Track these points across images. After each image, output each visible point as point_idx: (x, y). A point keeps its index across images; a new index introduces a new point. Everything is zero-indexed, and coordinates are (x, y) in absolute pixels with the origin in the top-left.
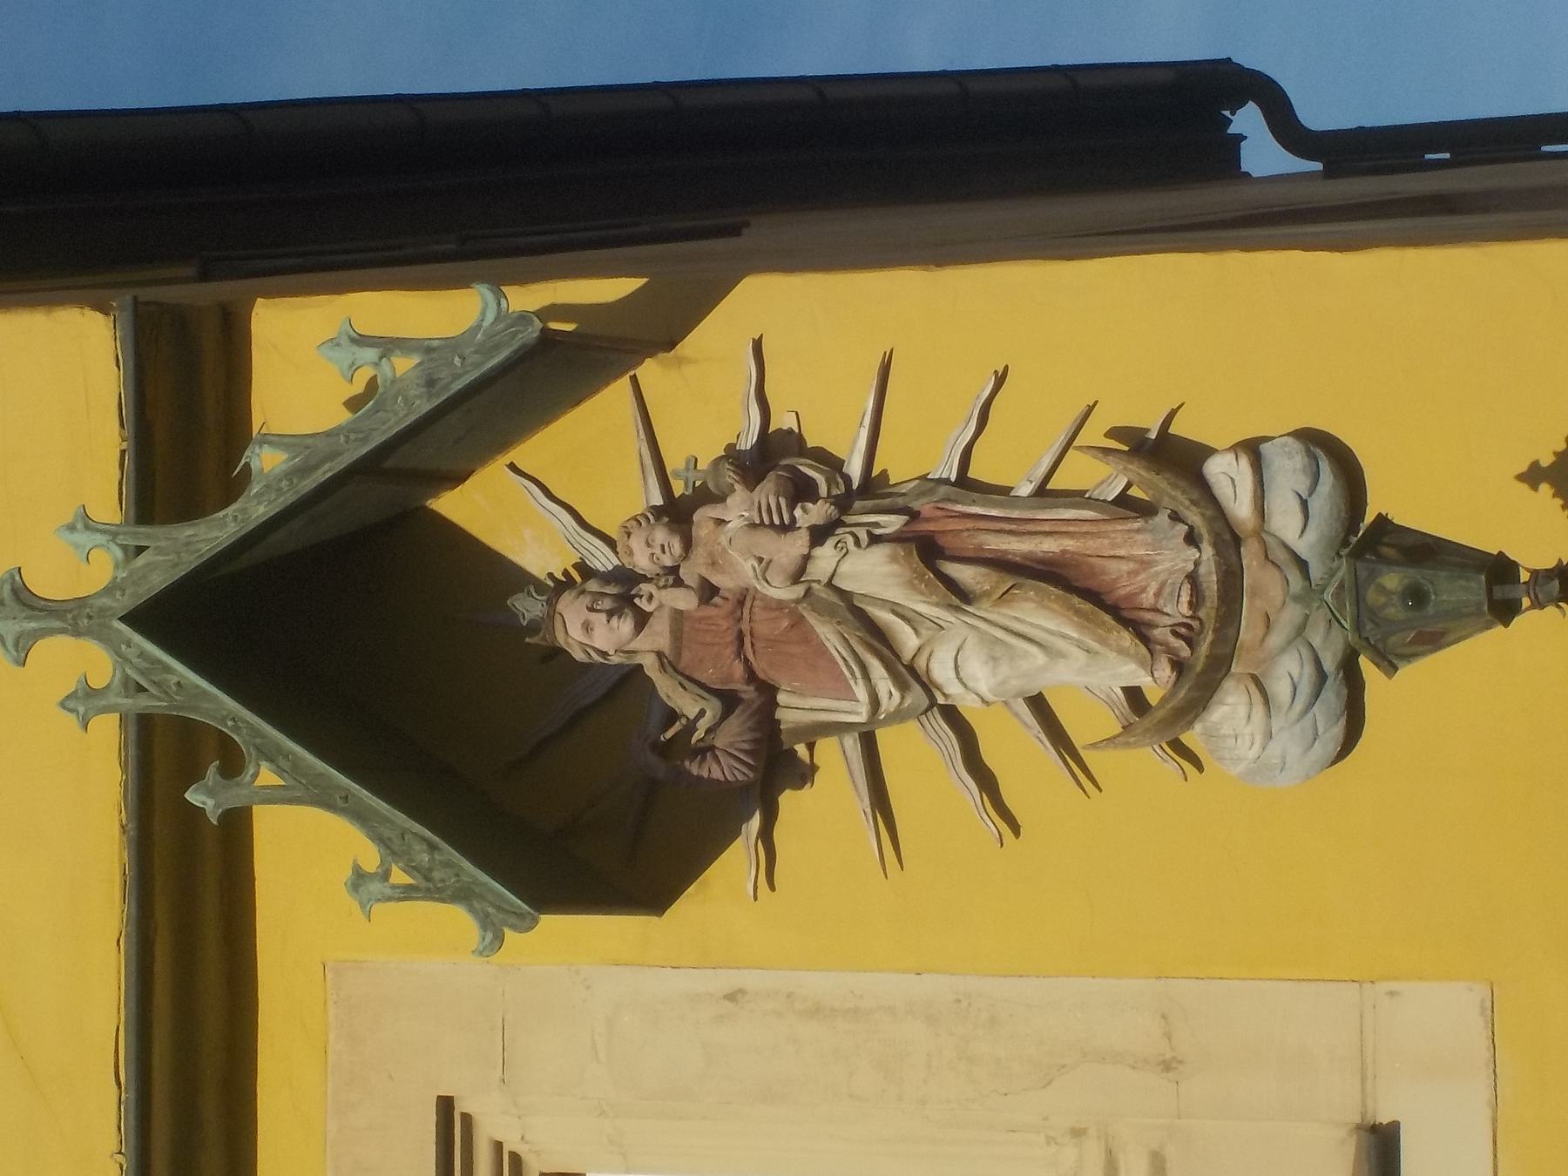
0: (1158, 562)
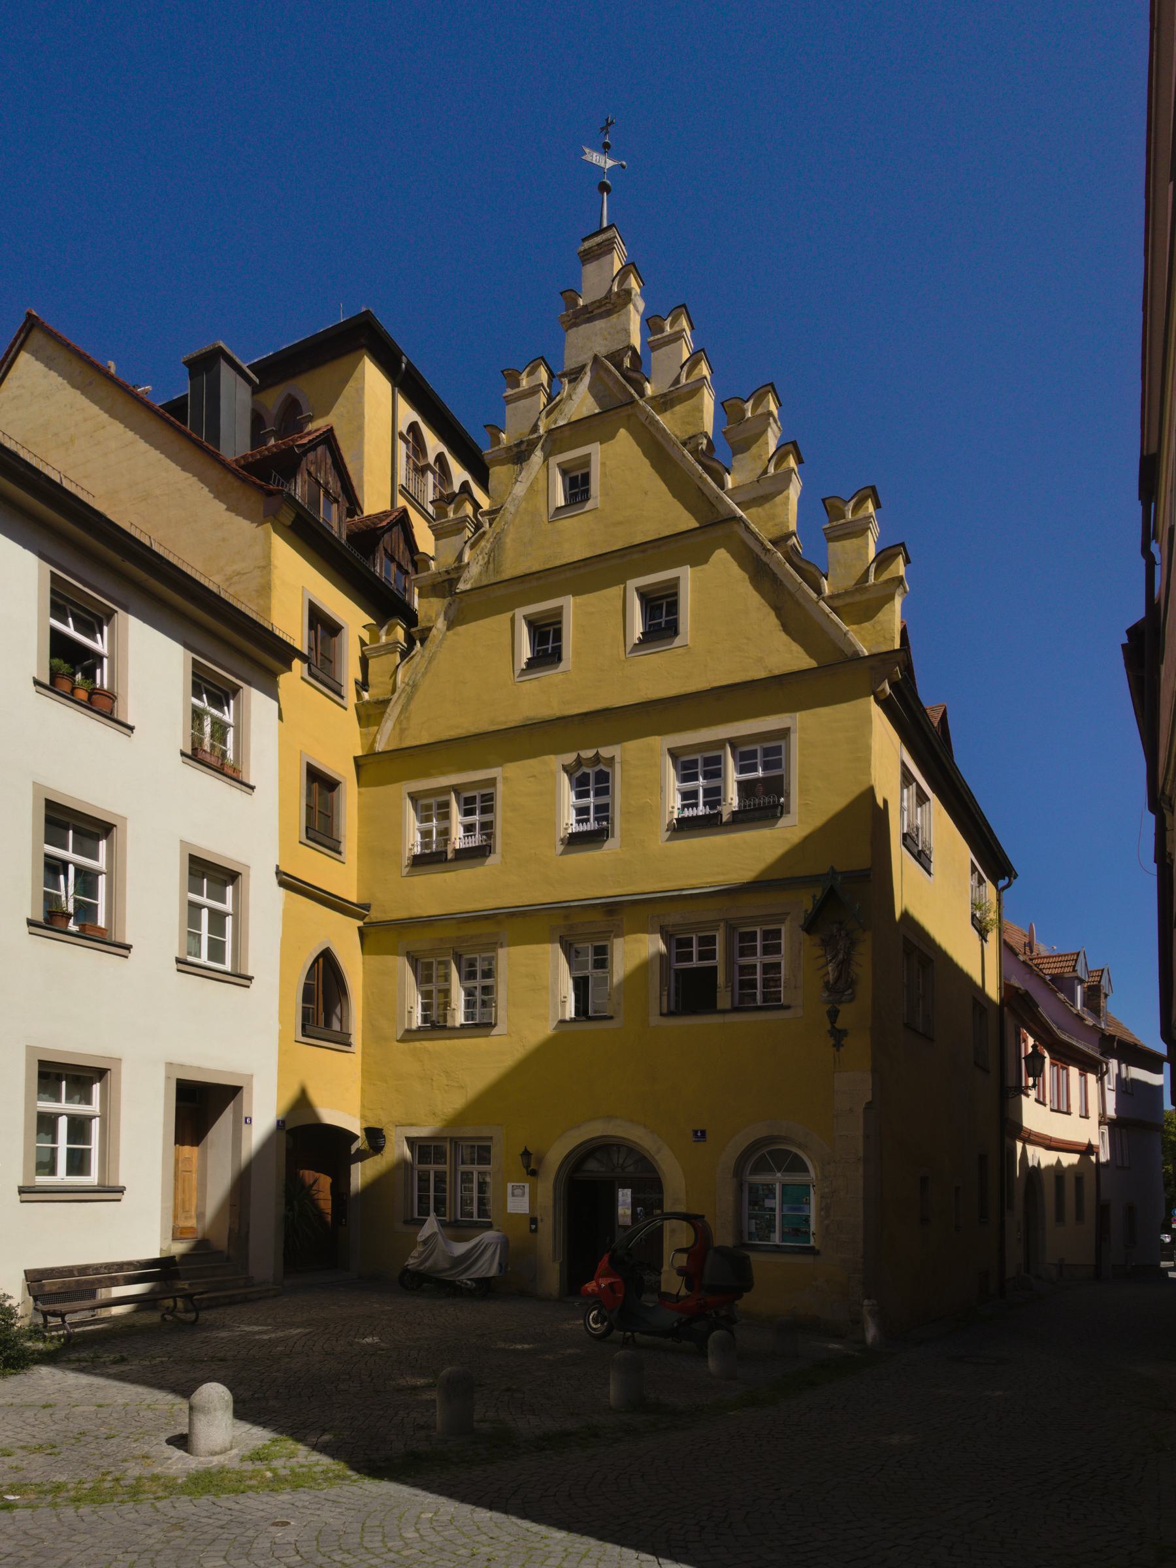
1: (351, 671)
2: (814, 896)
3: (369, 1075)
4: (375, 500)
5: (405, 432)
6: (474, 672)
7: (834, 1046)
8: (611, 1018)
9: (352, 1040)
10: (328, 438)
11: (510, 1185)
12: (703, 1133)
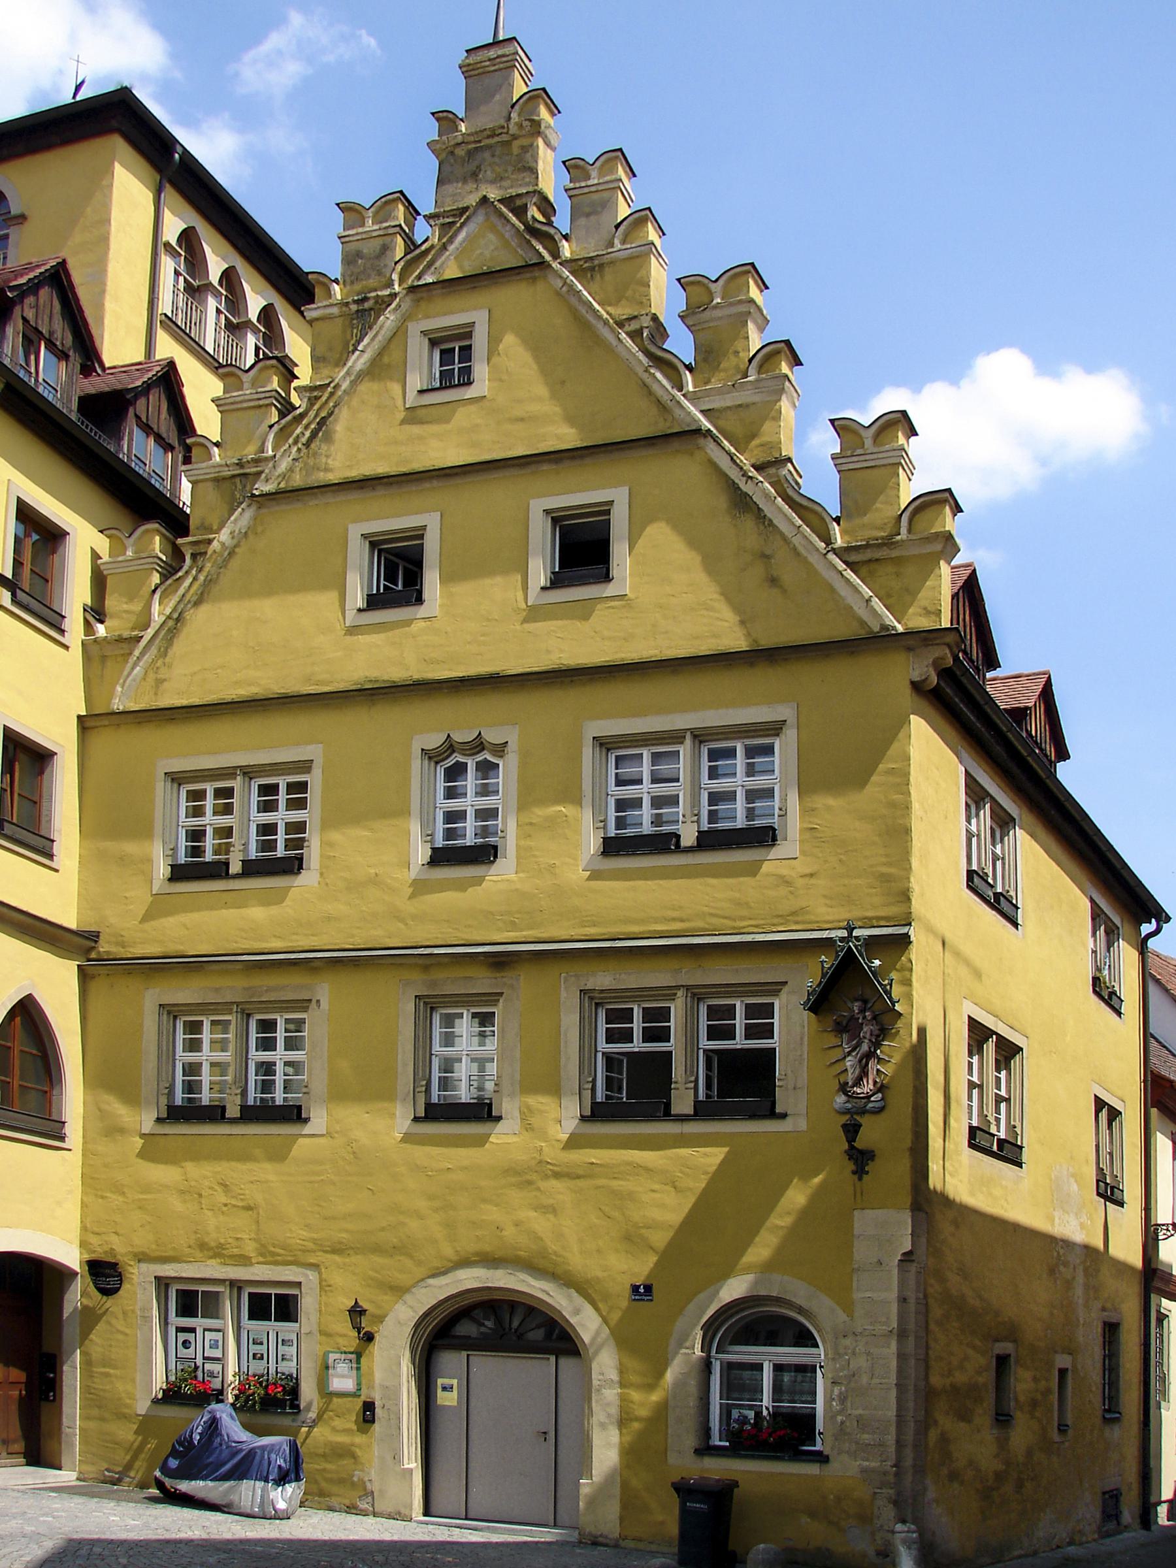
1: (76, 592)
3: (94, 1181)
4: (121, 344)
5: (174, 243)
6: (285, 626)
7: (854, 1173)
9: (67, 1129)
10: (58, 279)
12: (648, 1289)
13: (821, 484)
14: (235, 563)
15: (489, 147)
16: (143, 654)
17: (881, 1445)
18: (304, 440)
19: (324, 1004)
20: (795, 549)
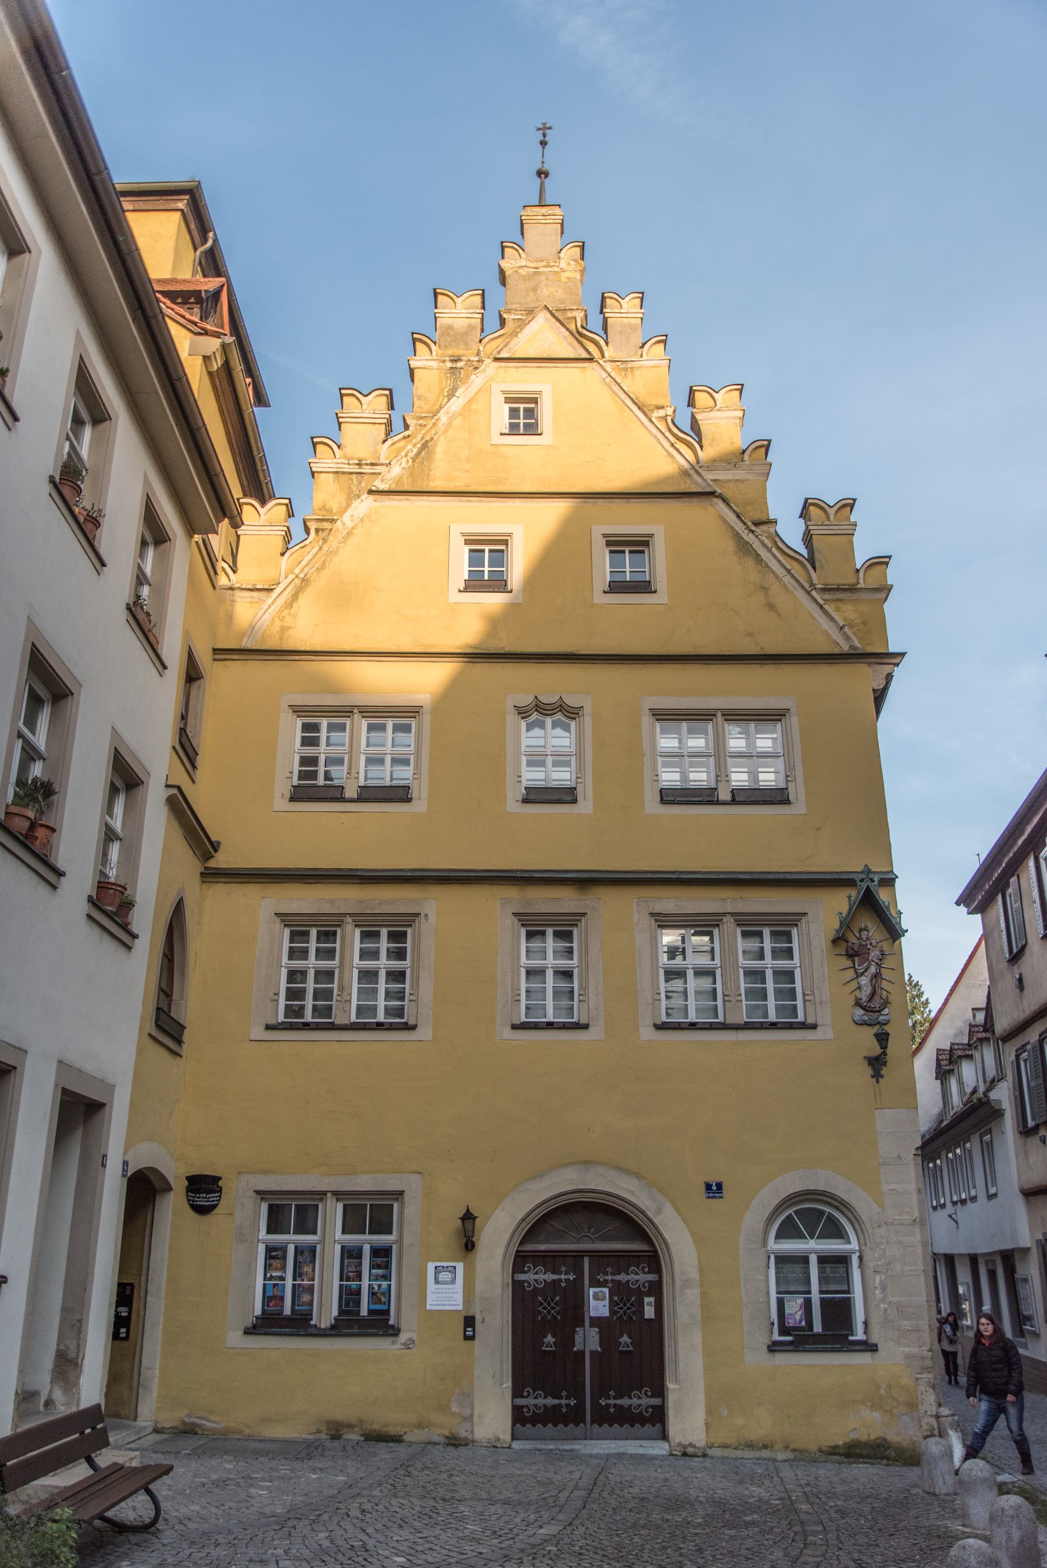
0: (876, 1004)
2: (849, 897)
8: (586, 1027)
11: (431, 1266)
12: (719, 1186)
13: (791, 531)
14: (351, 541)
15: (545, 273)
16: (273, 603)
17: (918, 1330)
18: (412, 455)
19: (432, 918)
20: (785, 586)
